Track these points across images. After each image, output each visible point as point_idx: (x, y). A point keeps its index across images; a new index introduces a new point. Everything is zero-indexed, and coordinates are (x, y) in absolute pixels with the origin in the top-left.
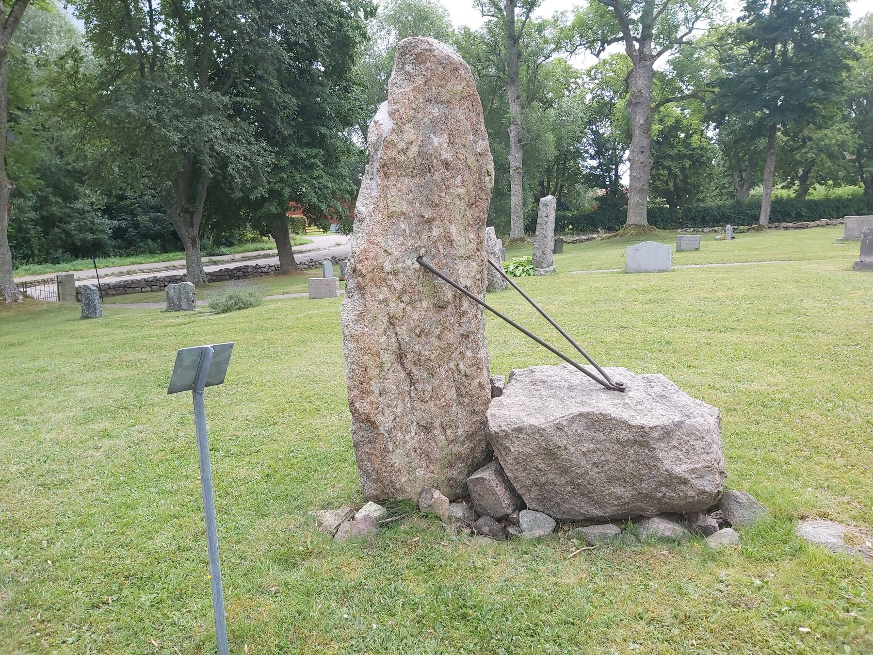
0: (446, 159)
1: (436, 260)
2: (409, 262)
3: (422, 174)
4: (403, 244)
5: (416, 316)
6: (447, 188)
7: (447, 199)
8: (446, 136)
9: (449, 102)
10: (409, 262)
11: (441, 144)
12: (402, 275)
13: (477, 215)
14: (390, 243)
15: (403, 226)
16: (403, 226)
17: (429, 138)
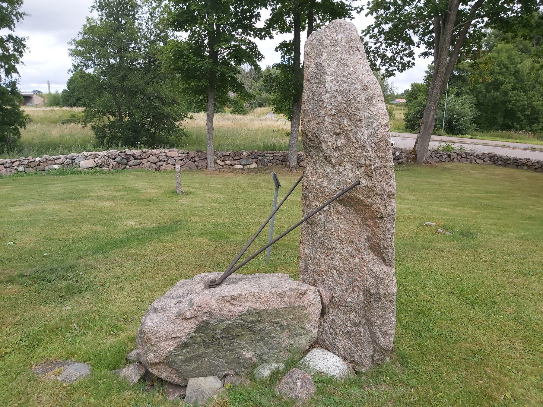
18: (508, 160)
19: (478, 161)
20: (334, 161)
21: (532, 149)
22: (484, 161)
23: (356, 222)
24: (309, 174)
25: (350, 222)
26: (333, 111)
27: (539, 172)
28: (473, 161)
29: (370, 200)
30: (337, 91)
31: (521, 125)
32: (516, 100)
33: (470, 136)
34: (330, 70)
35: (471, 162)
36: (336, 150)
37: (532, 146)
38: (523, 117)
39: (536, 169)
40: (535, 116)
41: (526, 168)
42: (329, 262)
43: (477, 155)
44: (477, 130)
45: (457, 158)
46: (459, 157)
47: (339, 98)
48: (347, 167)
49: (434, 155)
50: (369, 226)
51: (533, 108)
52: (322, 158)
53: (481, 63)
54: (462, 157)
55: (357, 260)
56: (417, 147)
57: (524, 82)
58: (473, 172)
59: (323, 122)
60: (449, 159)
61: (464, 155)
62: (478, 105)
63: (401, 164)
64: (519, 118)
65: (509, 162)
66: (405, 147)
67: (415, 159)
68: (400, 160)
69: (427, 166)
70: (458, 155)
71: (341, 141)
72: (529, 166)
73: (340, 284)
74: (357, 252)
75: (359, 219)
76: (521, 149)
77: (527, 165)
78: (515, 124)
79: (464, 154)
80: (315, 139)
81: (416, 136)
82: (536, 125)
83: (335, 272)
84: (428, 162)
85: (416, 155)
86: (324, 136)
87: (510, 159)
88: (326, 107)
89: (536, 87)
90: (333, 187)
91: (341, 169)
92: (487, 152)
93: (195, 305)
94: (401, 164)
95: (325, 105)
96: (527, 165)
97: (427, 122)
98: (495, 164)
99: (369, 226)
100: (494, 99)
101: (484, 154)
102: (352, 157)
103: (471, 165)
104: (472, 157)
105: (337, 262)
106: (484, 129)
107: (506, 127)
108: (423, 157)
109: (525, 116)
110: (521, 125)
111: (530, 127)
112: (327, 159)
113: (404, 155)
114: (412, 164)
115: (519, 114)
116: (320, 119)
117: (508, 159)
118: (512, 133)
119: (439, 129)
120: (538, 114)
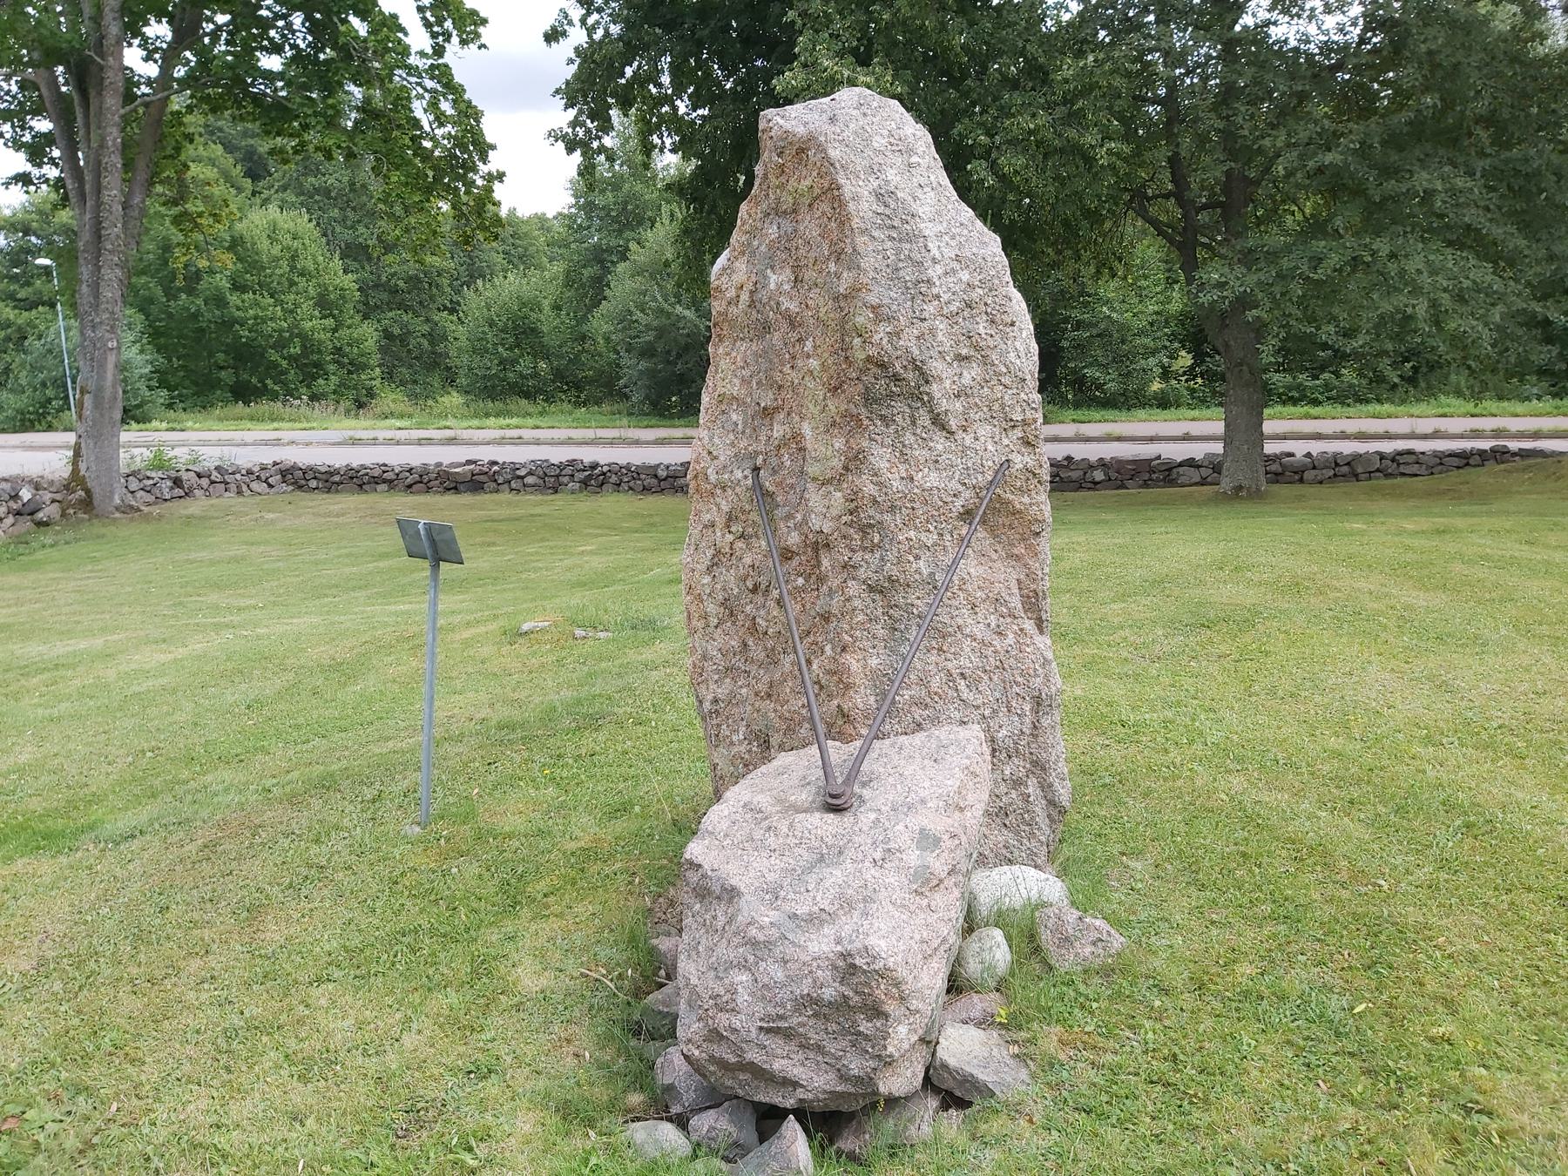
0: (787, 309)
1: (778, 478)
2: (739, 474)
3: (761, 337)
4: (733, 444)
5: (748, 560)
6: (794, 358)
7: (794, 376)
8: (788, 271)
9: (795, 211)
10: (739, 474)
11: (780, 285)
12: (729, 491)
13: (843, 407)
14: (716, 440)
15: (734, 417)
16: (734, 417)
17: (766, 277)
18: (331, 474)
19: (254, 485)
20: (953, 424)
21: (355, 442)
22: (271, 486)
23: (995, 556)
24: (884, 465)
25: (983, 560)
26: (953, 308)
27: (419, 492)
28: (244, 488)
29: (1026, 500)
30: (958, 259)
31: (284, 384)
32: (256, 318)
33: (164, 425)
34: (924, 210)
35: (240, 493)
36: (958, 396)
37: (351, 433)
38: (284, 363)
39: (410, 486)
40: (315, 357)
41: (384, 487)
42: (949, 665)
43: (250, 472)
44: (170, 406)
45: (200, 487)
46: (205, 482)
47: (965, 276)
48: (981, 432)
49: (134, 485)
50: (1018, 558)
51: (303, 337)
52: (924, 419)
53: (200, 215)
54: (213, 482)
55: (1011, 639)
56: (82, 466)
57: (264, 269)
58: (271, 516)
59: (932, 331)
60: (178, 492)
61: (215, 476)
62: (157, 336)
63: (46, 524)
64: (275, 365)
65: (337, 478)
66: (27, 473)
67: (87, 504)
68: (40, 515)
69: (132, 520)
70: (199, 476)
71: (970, 374)
72: (391, 481)
73: (978, 707)
74: (1009, 620)
75: (998, 547)
76: (339, 444)
77: (385, 481)
78: (268, 381)
79: (215, 473)
80: (910, 375)
81: (71, 438)
82: (321, 381)
83: (962, 684)
84: (131, 507)
85: (88, 492)
86: (936, 366)
87: (337, 472)
88: (938, 297)
89: (296, 284)
90: (954, 485)
91: (968, 440)
92: (268, 461)
93: (945, 837)
94: (46, 524)
95: (935, 291)
96: (385, 481)
97: (100, 389)
98: (300, 487)
99: (1018, 558)
100: (195, 316)
101: (263, 468)
102: (996, 407)
103: (241, 499)
104: (238, 476)
105: (967, 659)
106: (188, 404)
107: (243, 393)
108: (112, 493)
109: (290, 358)
110: (284, 384)
111: (309, 387)
112: (939, 422)
113: (47, 497)
114: (83, 520)
115: (273, 355)
116: (926, 324)
117: (332, 473)
118: (265, 407)
119: (60, 410)
120: (320, 352)
